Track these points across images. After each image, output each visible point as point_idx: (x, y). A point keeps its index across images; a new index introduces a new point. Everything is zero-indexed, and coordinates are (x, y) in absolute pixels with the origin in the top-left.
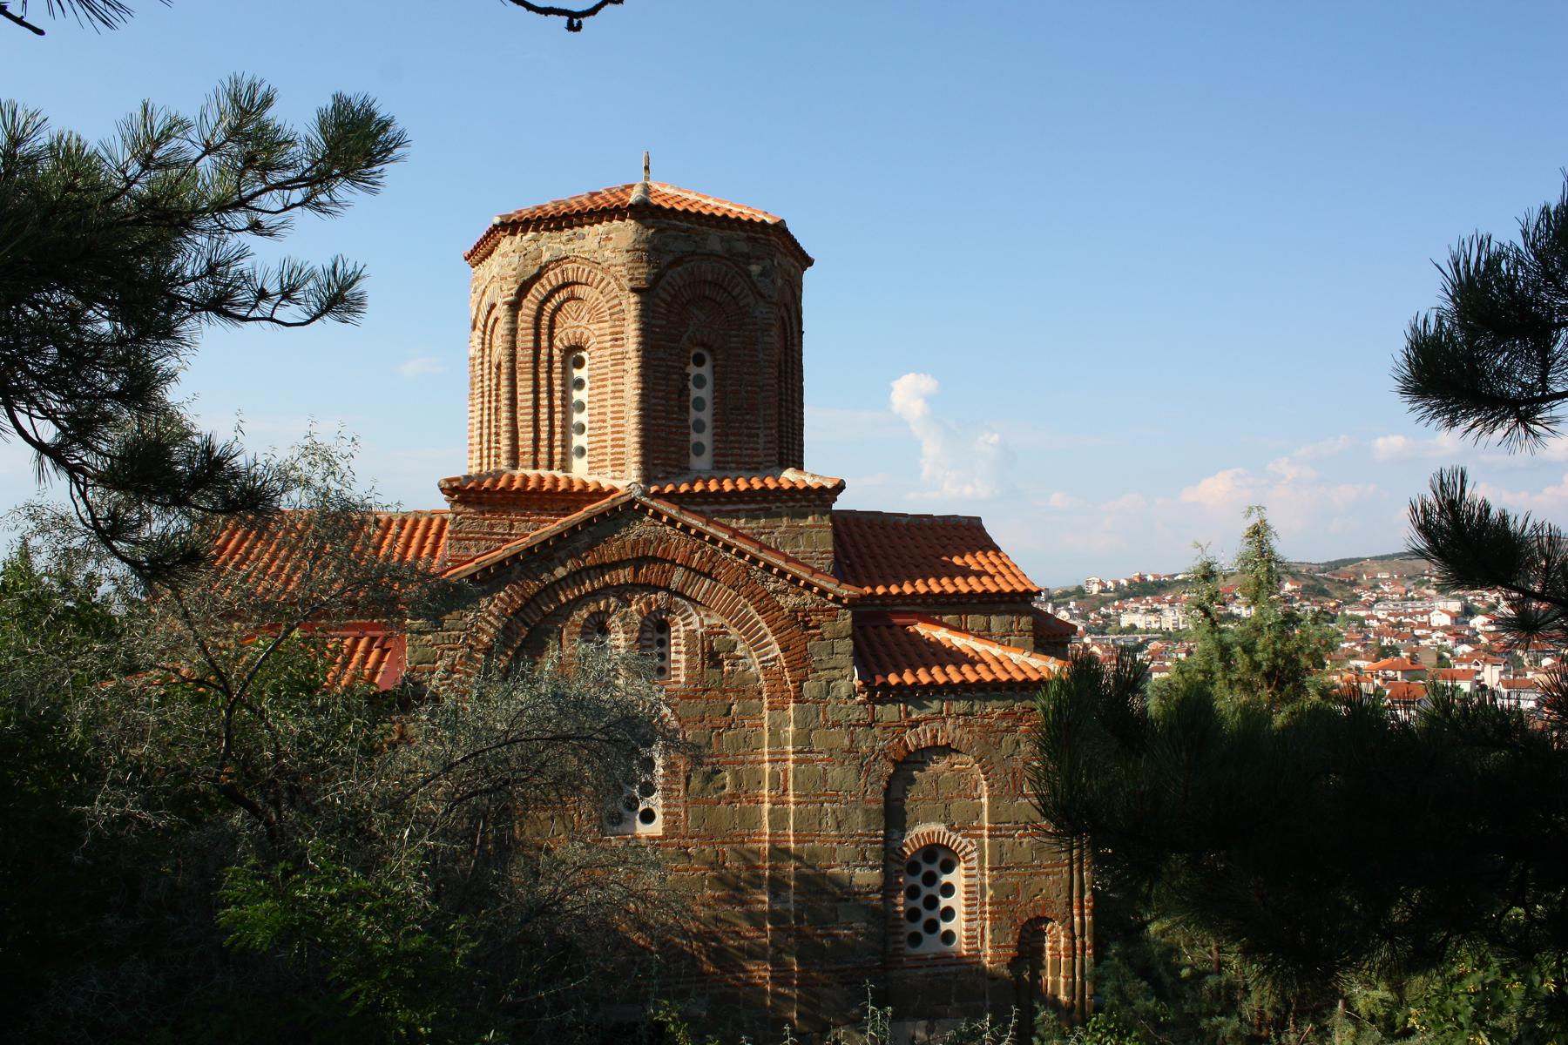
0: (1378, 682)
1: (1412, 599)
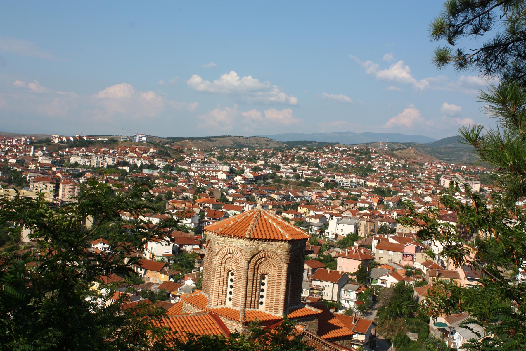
0: (201, 208)
1: (207, 162)
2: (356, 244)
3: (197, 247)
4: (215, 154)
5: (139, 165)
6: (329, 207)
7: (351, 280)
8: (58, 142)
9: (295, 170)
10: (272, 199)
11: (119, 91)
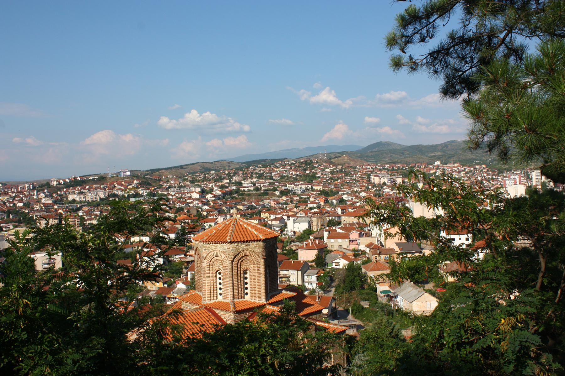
1: (182, 186)
2: (311, 237)
3: (183, 256)
4: (187, 179)
5: (126, 195)
6: (286, 210)
8: (57, 185)
9: (254, 184)
10: (238, 210)
11: (102, 137)
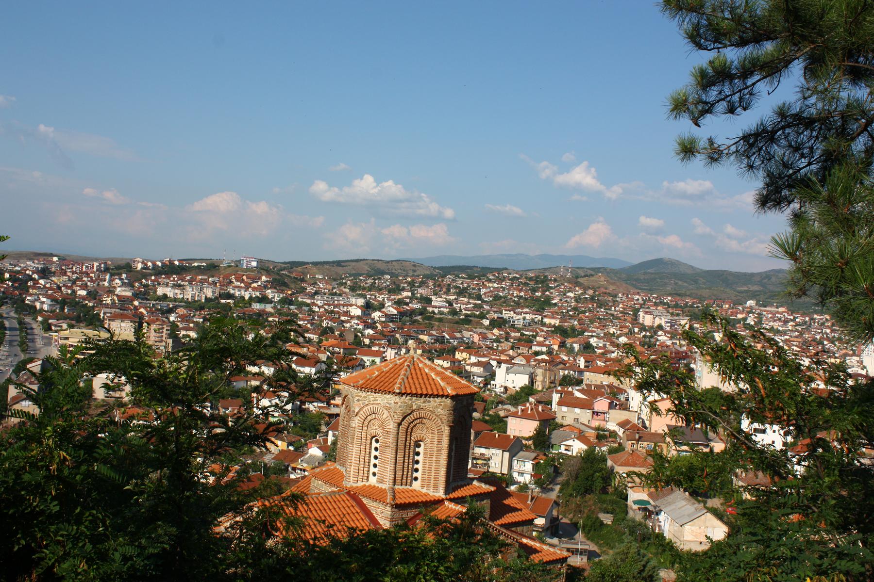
1: (335, 294)
2: (531, 400)
4: (346, 283)
7: (526, 446)
8: (142, 268)
9: (451, 304)
10: (421, 342)
11: (221, 202)
